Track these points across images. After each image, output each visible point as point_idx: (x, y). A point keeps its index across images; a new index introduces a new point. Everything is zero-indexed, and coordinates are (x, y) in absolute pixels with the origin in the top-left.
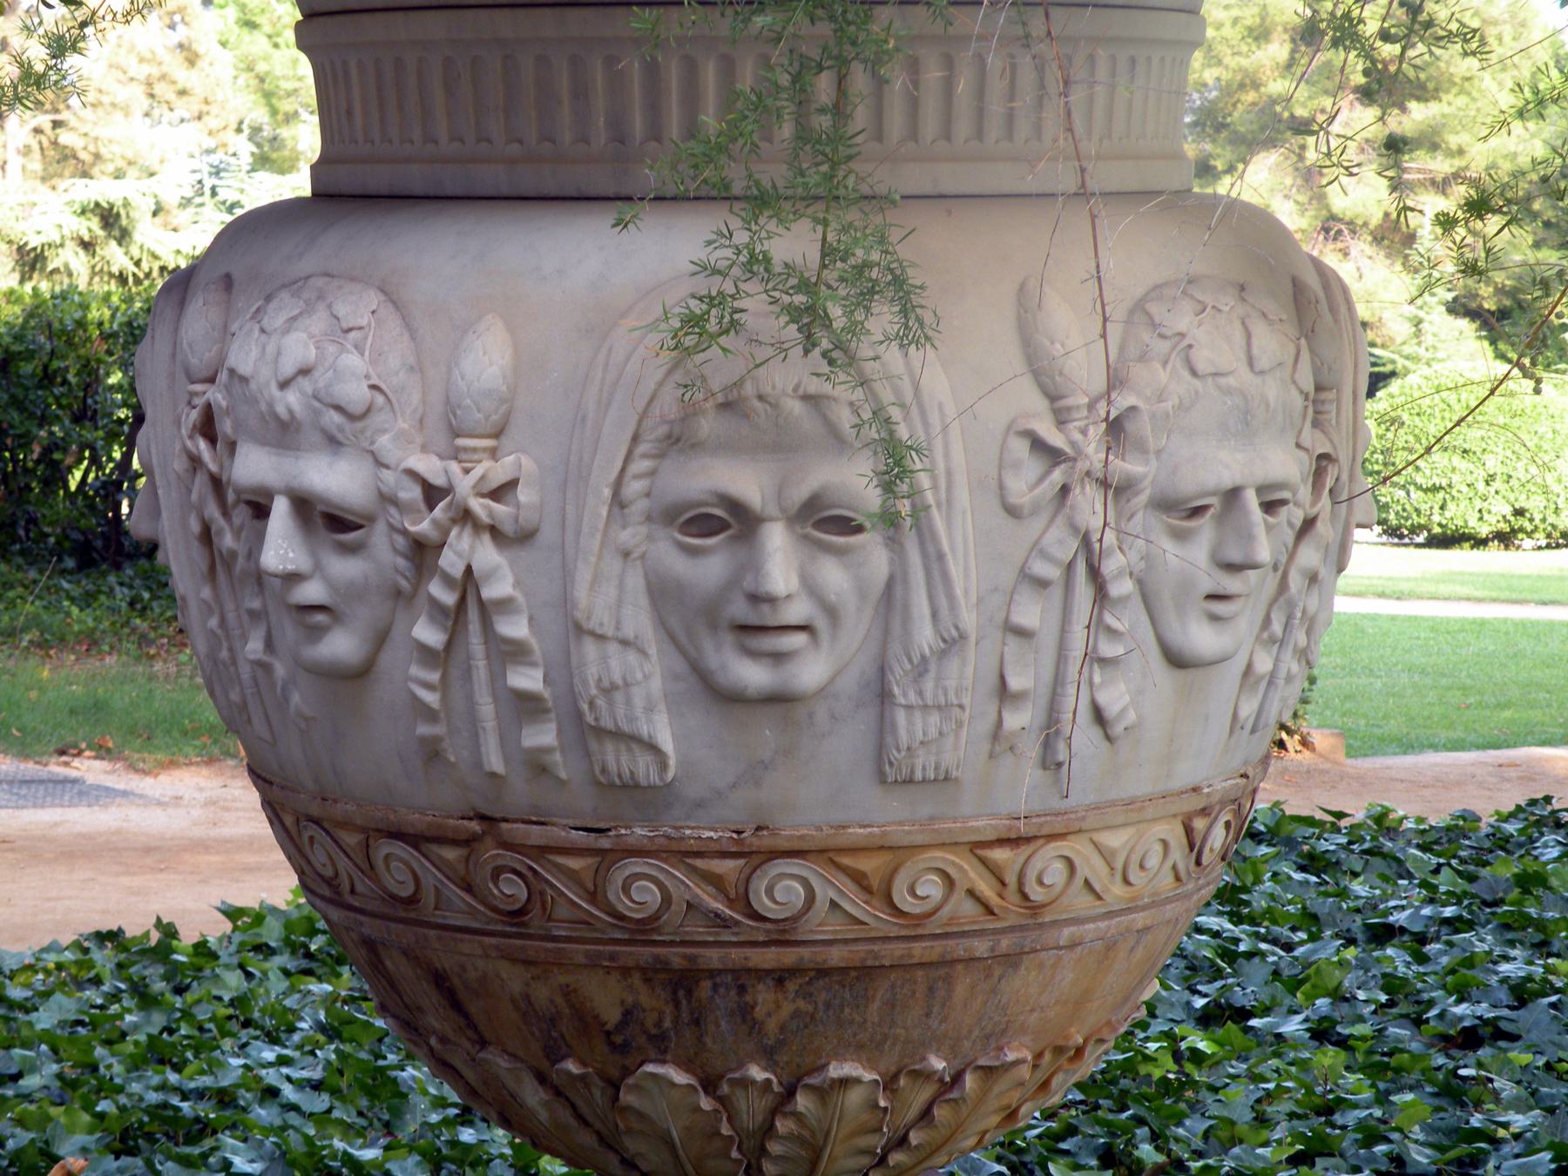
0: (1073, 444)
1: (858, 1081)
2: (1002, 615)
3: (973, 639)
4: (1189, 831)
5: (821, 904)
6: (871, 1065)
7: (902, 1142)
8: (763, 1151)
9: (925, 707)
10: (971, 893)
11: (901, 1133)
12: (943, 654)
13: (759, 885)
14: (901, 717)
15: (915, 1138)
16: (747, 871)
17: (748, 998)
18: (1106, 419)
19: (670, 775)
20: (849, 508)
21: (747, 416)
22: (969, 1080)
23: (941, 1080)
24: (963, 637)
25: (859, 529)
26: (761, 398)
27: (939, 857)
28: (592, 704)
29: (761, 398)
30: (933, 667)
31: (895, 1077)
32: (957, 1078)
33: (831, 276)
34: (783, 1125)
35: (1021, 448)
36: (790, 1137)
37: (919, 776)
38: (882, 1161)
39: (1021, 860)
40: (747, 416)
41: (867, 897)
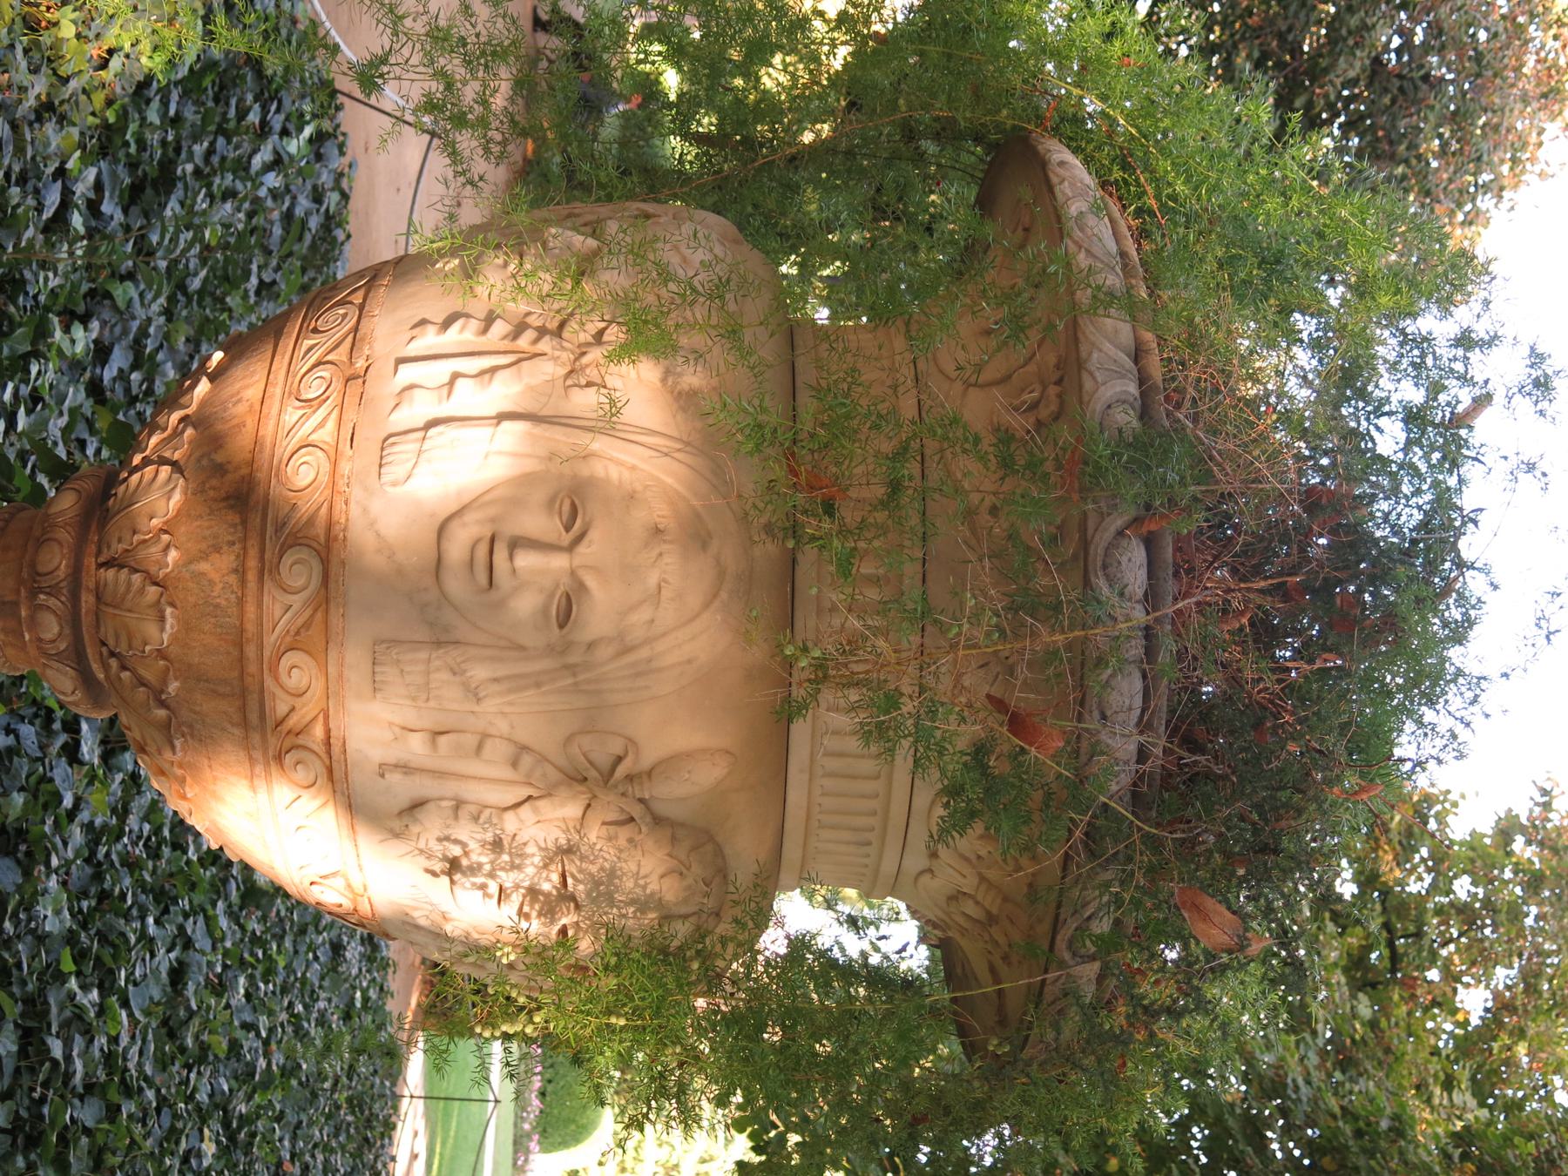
0: (616, 786)
1: (162, 630)
2: (492, 731)
3: (476, 708)
4: (334, 874)
5: (291, 599)
6: (174, 639)
7: (124, 668)
8: (121, 567)
9: (428, 673)
10: (293, 709)
11: (129, 665)
12: (465, 686)
13: (303, 554)
14: (423, 655)
15: (125, 675)
16: (315, 545)
17: (225, 548)
18: (1341, 935)
19: (389, 489)
20: (551, 596)
21: (646, 545)
22: (162, 713)
23: (162, 691)
24: (479, 700)
25: (561, 626)
26: (661, 554)
27: (318, 688)
28: (647, 687)
29: (661, 554)
30: (457, 679)
31: (164, 658)
32: (163, 704)
33: (732, 307)
34: (136, 578)
35: (616, 747)
36: (129, 584)
37: (377, 669)
38: (112, 654)
39: (315, 748)
40: (646, 545)
41: (293, 629)
